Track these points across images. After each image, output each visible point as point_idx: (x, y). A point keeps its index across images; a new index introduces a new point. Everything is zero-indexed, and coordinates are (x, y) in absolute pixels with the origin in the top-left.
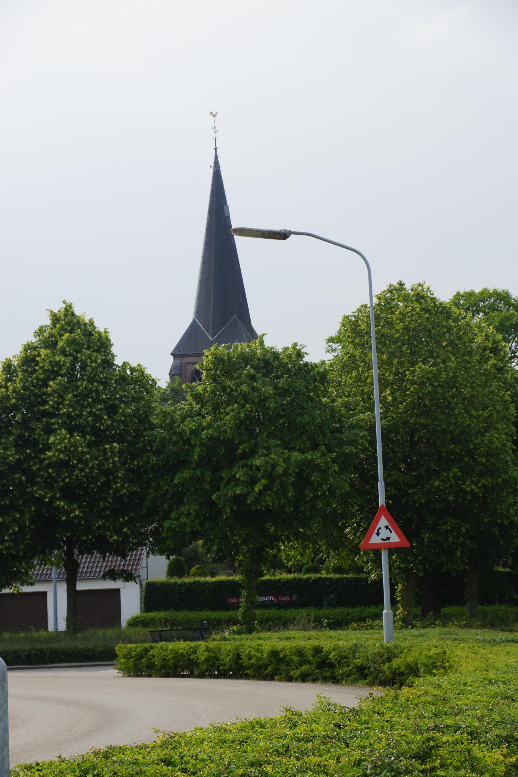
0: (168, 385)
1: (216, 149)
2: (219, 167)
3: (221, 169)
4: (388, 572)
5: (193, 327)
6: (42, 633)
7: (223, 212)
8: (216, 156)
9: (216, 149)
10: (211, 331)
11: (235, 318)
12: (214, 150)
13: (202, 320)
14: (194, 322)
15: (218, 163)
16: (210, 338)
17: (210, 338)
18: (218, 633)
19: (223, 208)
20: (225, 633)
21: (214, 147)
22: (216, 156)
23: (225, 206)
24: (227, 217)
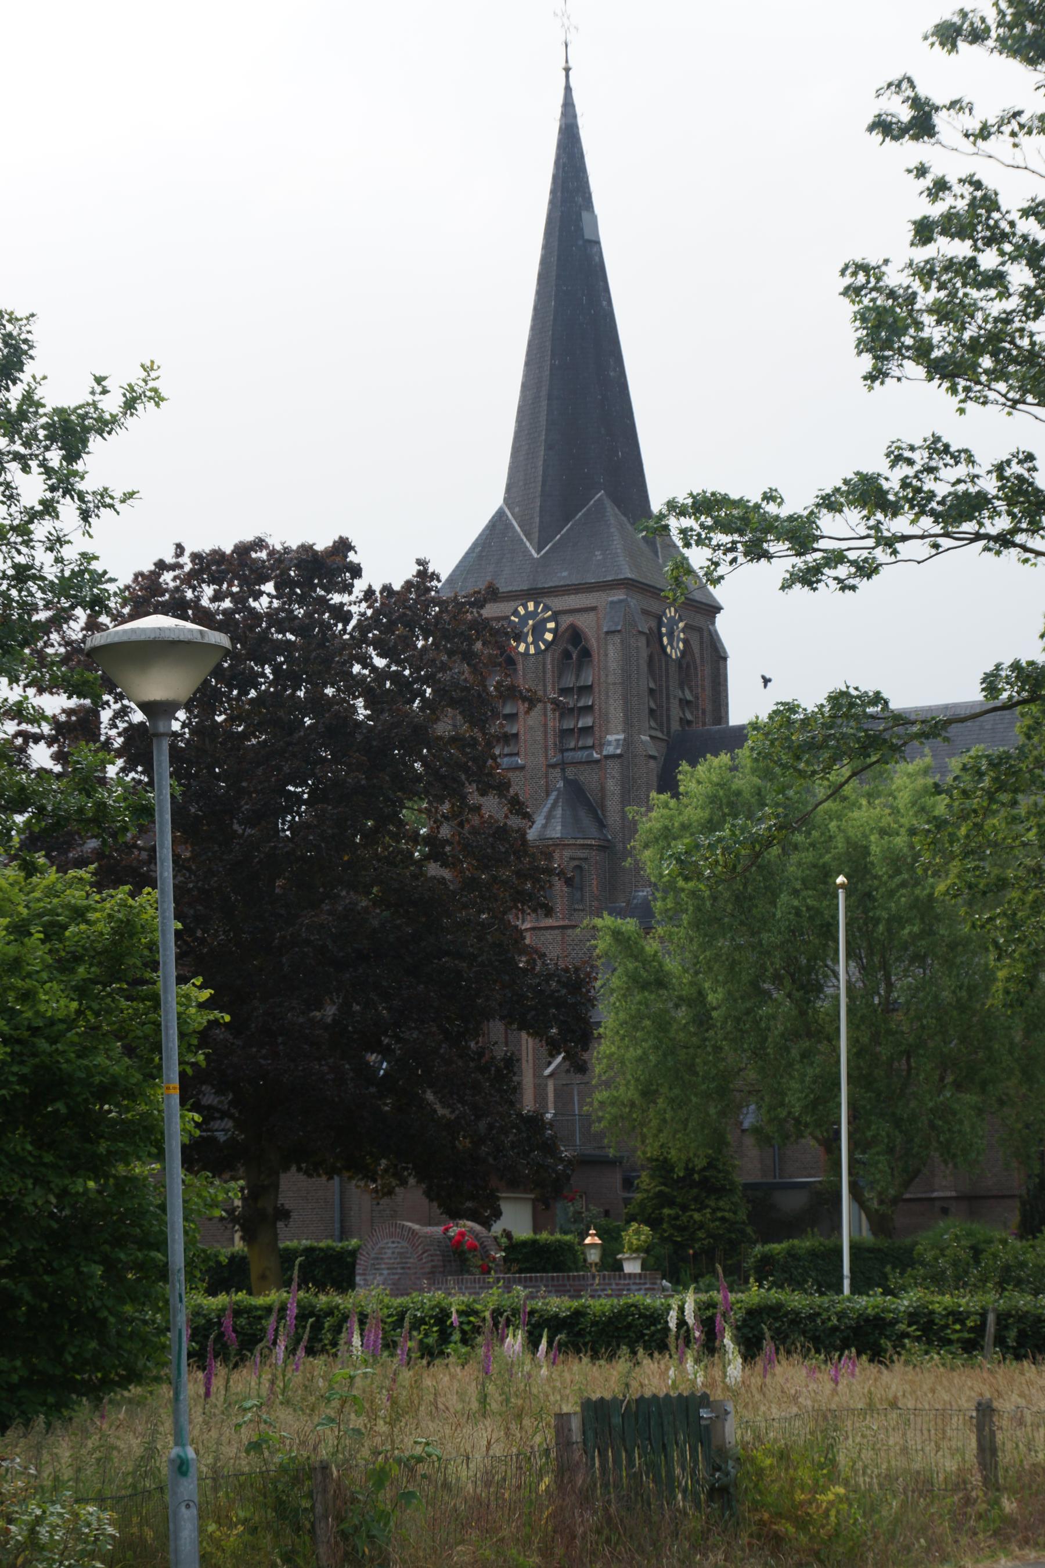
0: (662, 1395)
1: (567, 70)
2: (575, 116)
3: (581, 122)
4: (166, 1146)
5: (497, 526)
6: (841, 1297)
7: (579, 229)
8: (568, 89)
9: (567, 70)
10: (536, 536)
11: (599, 499)
12: (564, 73)
13: (517, 509)
14: (500, 514)
15: (573, 106)
16: (533, 552)
17: (533, 552)
18: (380, 1477)
19: (579, 218)
20: (1021, 770)
21: (563, 64)
22: (568, 89)
23: (585, 215)
24: (590, 241)
